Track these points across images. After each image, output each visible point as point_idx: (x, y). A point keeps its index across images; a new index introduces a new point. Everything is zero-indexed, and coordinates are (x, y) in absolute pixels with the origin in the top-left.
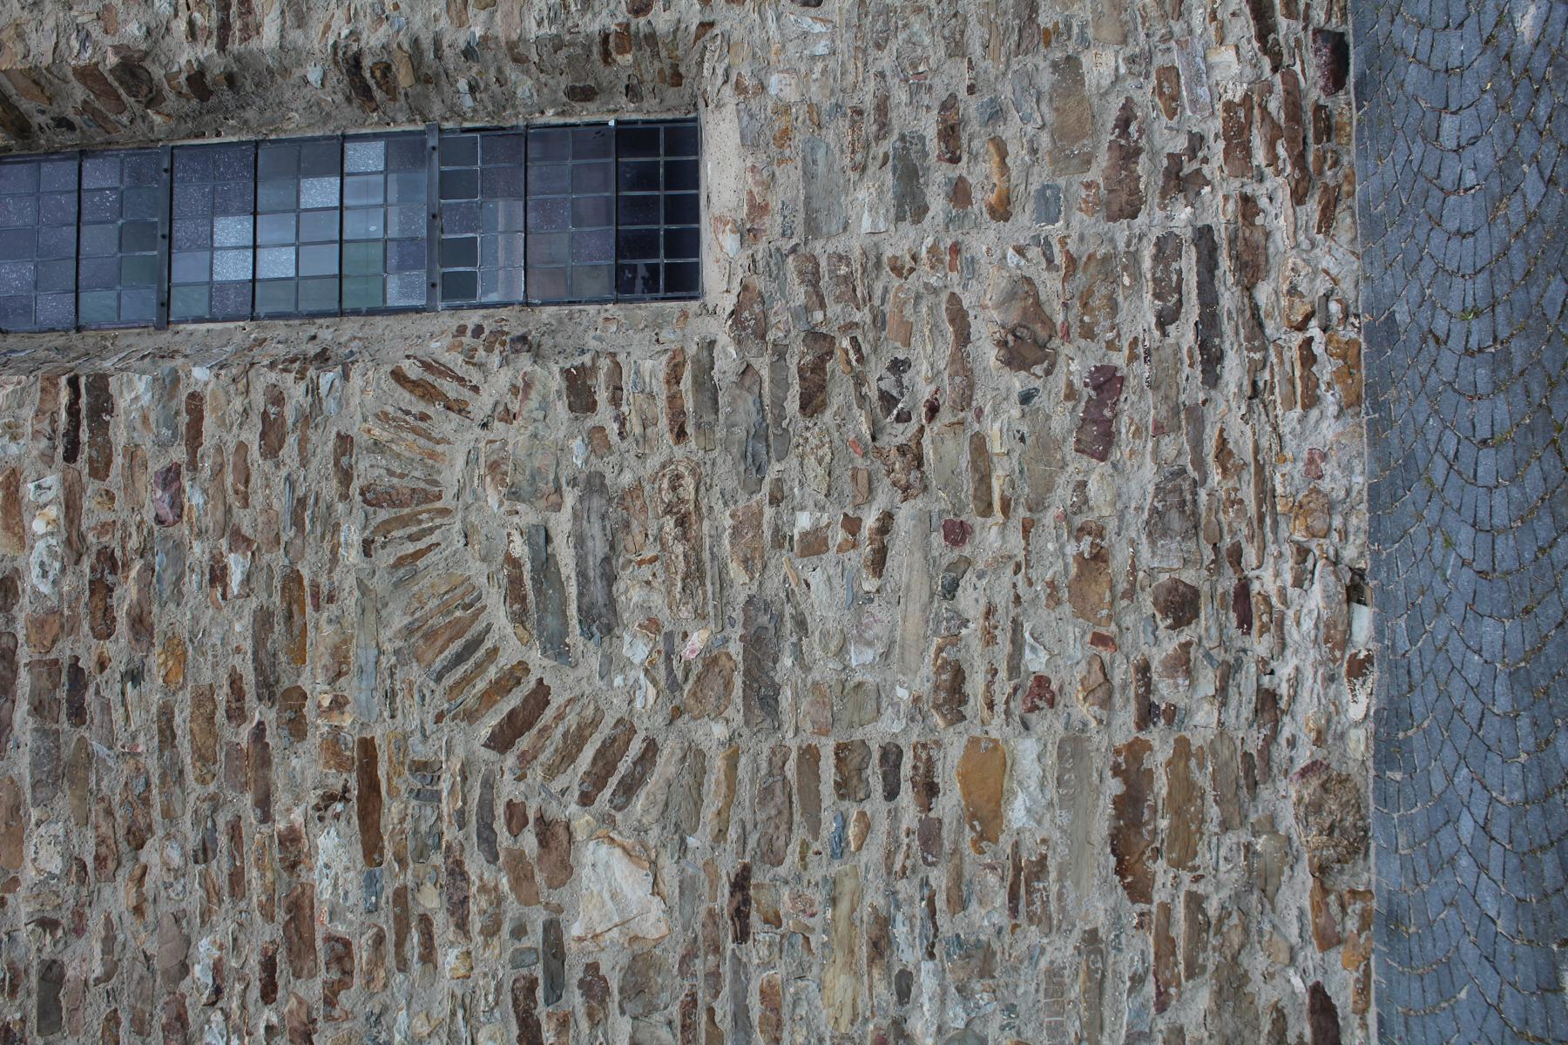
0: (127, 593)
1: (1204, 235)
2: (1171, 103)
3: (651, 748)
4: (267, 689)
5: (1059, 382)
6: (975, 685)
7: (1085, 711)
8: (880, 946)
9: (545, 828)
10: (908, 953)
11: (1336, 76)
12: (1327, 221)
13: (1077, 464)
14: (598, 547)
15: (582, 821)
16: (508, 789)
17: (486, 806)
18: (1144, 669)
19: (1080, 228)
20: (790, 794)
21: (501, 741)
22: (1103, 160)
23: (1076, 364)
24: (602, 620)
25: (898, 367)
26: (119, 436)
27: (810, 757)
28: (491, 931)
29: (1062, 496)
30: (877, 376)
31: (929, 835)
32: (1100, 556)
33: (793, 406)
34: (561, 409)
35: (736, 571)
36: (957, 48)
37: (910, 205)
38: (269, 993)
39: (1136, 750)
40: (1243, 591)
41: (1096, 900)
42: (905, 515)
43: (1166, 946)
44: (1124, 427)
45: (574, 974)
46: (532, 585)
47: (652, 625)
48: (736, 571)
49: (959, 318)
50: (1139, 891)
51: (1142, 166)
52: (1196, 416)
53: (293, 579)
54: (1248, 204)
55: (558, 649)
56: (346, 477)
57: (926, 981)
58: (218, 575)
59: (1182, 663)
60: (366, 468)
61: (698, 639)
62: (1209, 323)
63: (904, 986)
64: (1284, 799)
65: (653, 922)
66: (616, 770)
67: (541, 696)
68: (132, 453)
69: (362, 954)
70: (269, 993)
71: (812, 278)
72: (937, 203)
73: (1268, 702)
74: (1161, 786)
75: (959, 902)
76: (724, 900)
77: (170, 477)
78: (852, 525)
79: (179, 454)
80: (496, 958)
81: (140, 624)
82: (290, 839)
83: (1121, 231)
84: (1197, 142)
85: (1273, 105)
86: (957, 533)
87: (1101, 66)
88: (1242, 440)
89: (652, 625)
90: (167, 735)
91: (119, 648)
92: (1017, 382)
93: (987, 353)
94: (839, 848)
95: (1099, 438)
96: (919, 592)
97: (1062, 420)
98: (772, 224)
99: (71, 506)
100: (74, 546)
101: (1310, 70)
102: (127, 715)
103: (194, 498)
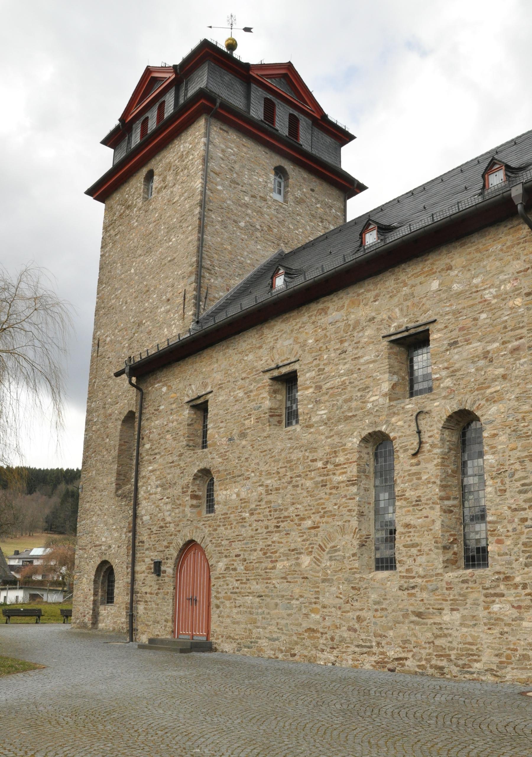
0: (334, 491)
1: (371, 647)
2: (387, 644)
3: (319, 566)
4: (325, 512)
5: (355, 624)
6: (325, 610)
7: (322, 625)
8: (301, 596)
9: (311, 552)
10: (301, 600)
11: (390, 670)
12: (372, 665)
13: (347, 625)
14: (338, 558)
15: (312, 557)
16: (315, 546)
17: (313, 544)
18: (326, 633)
19: (372, 628)
20: (315, 585)
21: (320, 546)
22: (380, 633)
23: (357, 626)
24: (331, 559)
25: (357, 600)
26: (350, 488)
27: (318, 587)
28: (302, 545)
29: (344, 623)
30: (356, 597)
31: (310, 603)
32: (337, 628)
33: (353, 585)
34: (352, 552)
35: (336, 577)
36: (393, 611)
37: (376, 603)
38: (296, 516)
39: (318, 631)
40: (334, 648)
41: (305, 625)
42: (342, 601)
43: (300, 634)
44: (350, 633)
45: (299, 556)
46: (334, 549)
47: (331, 566)
48: (336, 577)
49: (362, 610)
50: (306, 631)
51: (379, 638)
52: (352, 643)
53: (335, 515)
54: (375, 654)
55: (328, 553)
56: (345, 522)
57: (298, 602)
58: (336, 504)
59: (326, 639)
60: (347, 524)
61: (329, 572)
62: (362, 646)
63: (297, 599)
64: (314, 652)
65: (303, 566)
66: (317, 561)
67: (324, 551)
68: (348, 490)
69: (300, 528)
70: (296, 516)
71: (366, 588)
72: (375, 607)
73: (323, 651)
74: (315, 635)
75: (305, 607)
76: (306, 576)
77: (346, 496)
78: (341, 593)
79: (348, 497)
80: (299, 546)
81: (331, 494)
82: (310, 517)
83: (372, 634)
84: (383, 647)
85: (386, 659)
86: (340, 608)
87: (391, 633)
88: (350, 650)
89: (331, 566)
90: (320, 499)
91: (328, 491)
92: (355, 617)
93: (358, 613)
94: (310, 591)
95: (350, 629)
96: (334, 603)
97: (351, 624)
98: (372, 582)
99: (343, 482)
100: (339, 483)
101: (390, 666)
102: (322, 493)
103: (344, 500)
